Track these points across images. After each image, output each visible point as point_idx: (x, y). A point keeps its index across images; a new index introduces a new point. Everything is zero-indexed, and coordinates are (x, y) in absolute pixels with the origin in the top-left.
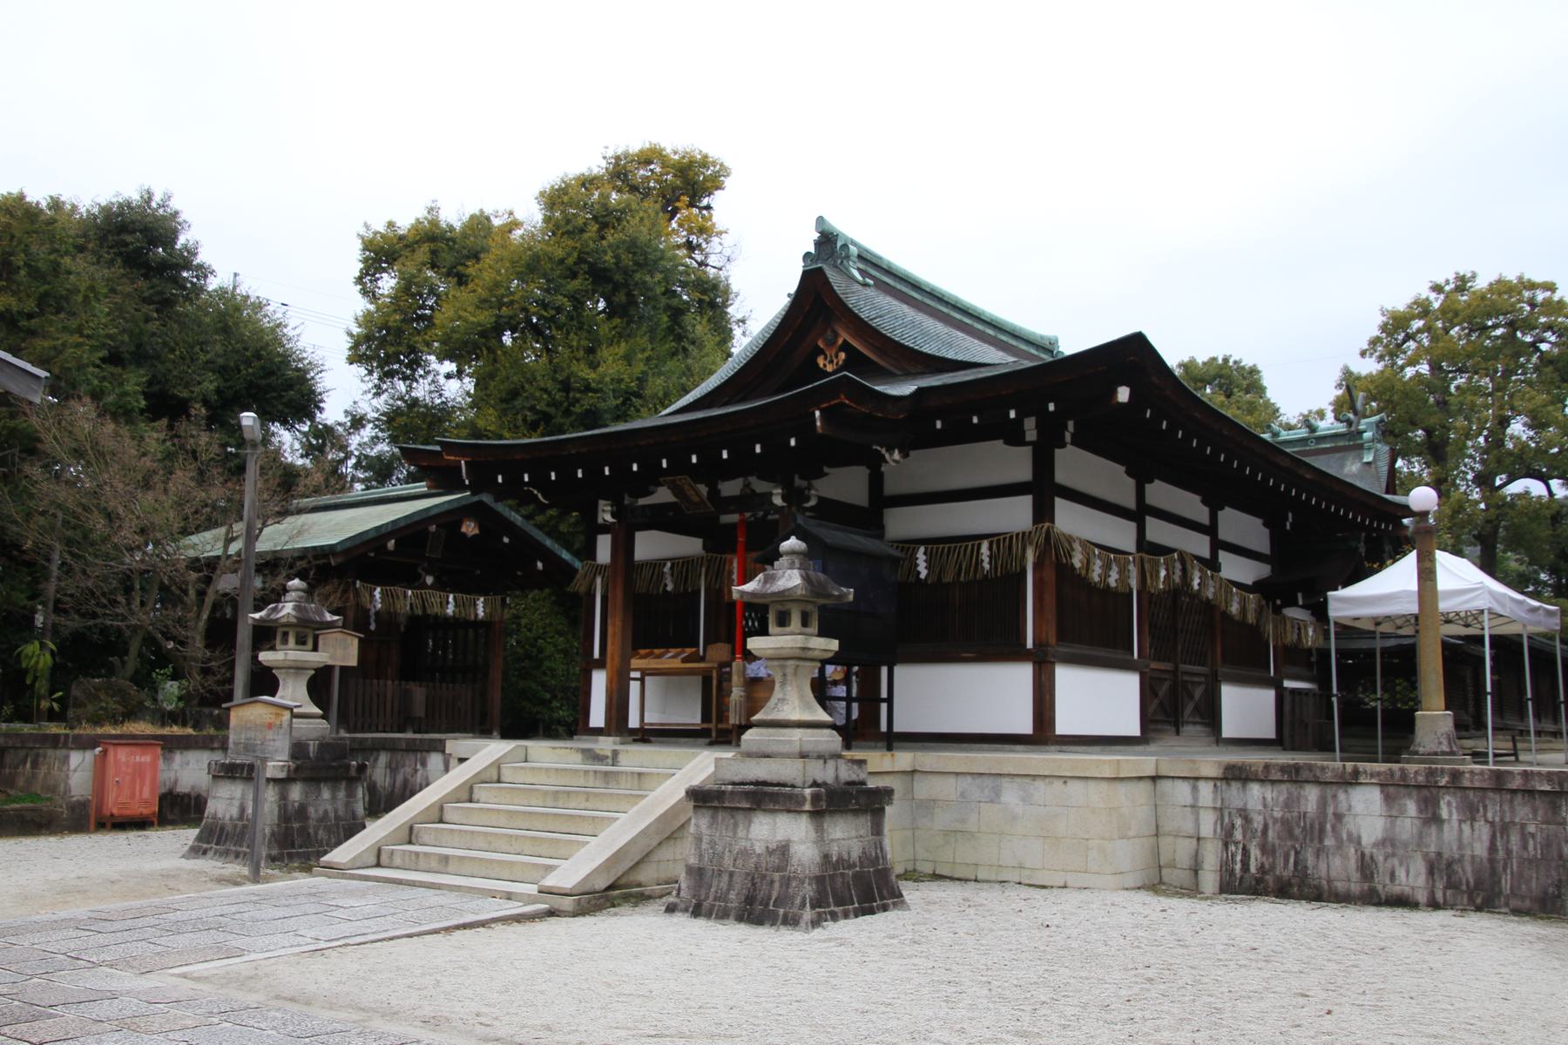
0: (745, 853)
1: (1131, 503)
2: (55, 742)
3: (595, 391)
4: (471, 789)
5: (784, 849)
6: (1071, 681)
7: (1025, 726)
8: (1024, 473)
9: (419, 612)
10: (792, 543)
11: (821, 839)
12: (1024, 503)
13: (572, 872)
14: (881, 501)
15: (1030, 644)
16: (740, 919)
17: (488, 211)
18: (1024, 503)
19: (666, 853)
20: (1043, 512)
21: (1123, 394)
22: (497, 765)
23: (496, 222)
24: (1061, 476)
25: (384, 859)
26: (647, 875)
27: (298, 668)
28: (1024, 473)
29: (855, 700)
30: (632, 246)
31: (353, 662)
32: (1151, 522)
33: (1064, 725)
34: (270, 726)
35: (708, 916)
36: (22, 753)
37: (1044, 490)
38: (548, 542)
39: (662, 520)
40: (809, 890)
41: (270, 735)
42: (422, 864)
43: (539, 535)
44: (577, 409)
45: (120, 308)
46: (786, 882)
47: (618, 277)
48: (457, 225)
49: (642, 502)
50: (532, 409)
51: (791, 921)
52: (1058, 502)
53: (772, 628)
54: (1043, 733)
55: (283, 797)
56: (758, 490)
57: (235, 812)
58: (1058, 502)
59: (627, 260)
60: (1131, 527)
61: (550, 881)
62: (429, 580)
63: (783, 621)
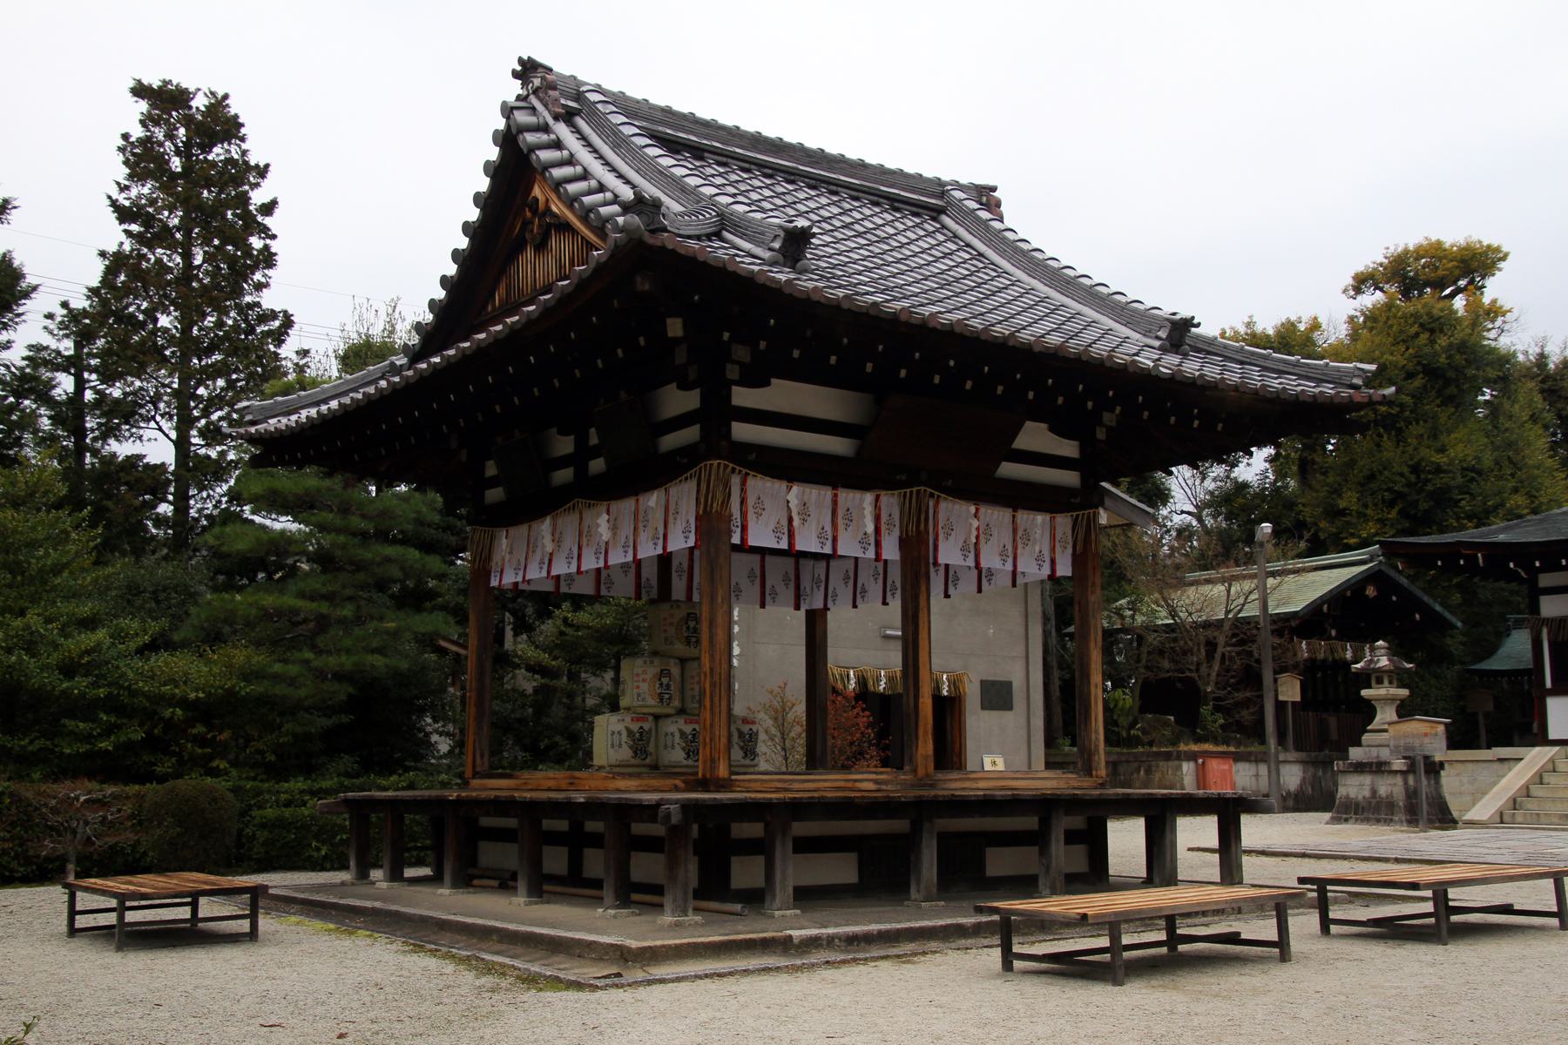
2: (1168, 756)
3: (1445, 472)
4: (1541, 777)
17: (1293, 318)
22: (1552, 760)
23: (1302, 327)
25: (1506, 818)
27: (1388, 700)
29: (121, 917)
30: (1462, 347)
31: (1298, 699)
33: (1549, 884)
34: (1426, 735)
36: (1136, 765)
38: (1426, 598)
41: (1427, 740)
42: (1543, 820)
43: (1419, 593)
44: (1429, 487)
45: (1376, 505)
47: (1451, 374)
48: (1271, 332)
50: (1389, 490)
55: (1406, 783)
56: (554, 209)
57: (1367, 793)
59: (1459, 359)
62: (1333, 633)
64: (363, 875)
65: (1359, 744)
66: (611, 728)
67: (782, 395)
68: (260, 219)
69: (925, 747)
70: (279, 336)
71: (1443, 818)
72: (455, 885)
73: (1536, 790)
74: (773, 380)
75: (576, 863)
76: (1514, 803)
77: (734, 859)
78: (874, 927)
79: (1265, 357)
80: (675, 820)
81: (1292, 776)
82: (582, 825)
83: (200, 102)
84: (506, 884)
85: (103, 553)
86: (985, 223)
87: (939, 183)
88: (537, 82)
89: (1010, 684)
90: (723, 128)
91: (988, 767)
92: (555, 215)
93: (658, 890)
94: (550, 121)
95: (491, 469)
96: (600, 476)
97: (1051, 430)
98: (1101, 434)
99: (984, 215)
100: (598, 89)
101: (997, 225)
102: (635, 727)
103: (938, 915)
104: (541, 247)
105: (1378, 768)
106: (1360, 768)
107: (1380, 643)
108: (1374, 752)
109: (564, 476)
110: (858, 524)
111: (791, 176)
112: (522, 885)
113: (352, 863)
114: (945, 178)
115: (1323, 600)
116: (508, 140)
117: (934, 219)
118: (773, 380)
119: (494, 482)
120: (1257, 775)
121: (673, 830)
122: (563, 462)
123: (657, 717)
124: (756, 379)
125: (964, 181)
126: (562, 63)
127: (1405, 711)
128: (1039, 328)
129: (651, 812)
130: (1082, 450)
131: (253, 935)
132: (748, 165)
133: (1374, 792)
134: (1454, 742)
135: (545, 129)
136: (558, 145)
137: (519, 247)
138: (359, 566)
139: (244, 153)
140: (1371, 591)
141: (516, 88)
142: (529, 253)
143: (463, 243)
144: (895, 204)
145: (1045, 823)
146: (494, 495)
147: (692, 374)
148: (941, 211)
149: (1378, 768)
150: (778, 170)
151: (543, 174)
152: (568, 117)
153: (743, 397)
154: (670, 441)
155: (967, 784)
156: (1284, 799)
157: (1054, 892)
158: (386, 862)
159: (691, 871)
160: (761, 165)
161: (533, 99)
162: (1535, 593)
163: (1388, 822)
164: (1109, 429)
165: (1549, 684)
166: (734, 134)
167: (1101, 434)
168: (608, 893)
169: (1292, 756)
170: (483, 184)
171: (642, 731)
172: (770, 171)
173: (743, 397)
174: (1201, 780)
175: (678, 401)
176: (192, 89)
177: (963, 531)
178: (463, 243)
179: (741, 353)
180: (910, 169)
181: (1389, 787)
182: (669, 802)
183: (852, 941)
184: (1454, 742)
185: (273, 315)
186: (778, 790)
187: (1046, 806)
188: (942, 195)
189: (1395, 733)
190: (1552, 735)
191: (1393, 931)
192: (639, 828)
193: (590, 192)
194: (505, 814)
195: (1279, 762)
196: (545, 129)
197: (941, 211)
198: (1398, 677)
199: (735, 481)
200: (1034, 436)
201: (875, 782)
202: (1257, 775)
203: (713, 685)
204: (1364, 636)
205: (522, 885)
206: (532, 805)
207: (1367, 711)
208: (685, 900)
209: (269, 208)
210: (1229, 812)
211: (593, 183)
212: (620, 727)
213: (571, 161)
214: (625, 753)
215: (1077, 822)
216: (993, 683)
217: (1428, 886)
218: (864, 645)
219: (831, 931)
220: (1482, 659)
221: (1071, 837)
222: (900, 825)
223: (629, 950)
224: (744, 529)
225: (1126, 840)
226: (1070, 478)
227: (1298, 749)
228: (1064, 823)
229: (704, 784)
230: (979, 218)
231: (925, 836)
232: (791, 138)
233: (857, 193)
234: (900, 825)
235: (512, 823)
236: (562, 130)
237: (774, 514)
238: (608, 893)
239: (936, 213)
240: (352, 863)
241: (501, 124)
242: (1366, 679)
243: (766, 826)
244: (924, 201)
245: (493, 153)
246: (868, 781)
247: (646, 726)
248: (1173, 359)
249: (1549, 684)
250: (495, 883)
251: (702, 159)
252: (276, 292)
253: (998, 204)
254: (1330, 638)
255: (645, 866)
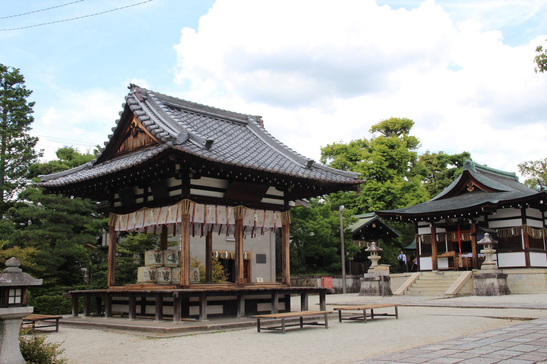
0: (485, 285)
1: (541, 217)
5: (493, 284)
6: (532, 255)
7: (524, 265)
8: (520, 214)
9: (168, 244)
10: (486, 234)
11: (498, 282)
12: (520, 220)
13: (451, 290)
14: (487, 220)
15: (523, 248)
16: (486, 295)
18: (520, 220)
19: (463, 289)
20: (524, 222)
21: (542, 202)
24: (527, 214)
26: (461, 292)
28: (520, 214)
32: (541, 226)
33: (532, 264)
35: (480, 295)
37: (524, 218)
39: (441, 226)
40: (498, 290)
46: (494, 289)
49: (437, 223)
51: (495, 295)
52: (527, 220)
53: (484, 248)
54: (528, 266)
55: (379, 284)
56: (140, 126)
57: (369, 287)
58: (527, 220)
60: (542, 222)
61: (447, 293)
63: (486, 246)
64: (76, 315)
65: (367, 273)
66: (144, 271)
67: (204, 181)
68: (29, 107)
69: (241, 275)
70: (33, 145)
71: (389, 293)
72: (108, 317)
73: (413, 285)
74: (202, 177)
75: (143, 310)
76: (408, 289)
77: (190, 307)
78: (228, 324)
79: (333, 170)
80: (177, 296)
81: (350, 282)
82: (145, 298)
83: (10, 70)
84: (124, 315)
85: (171, 260)
86: (259, 129)
87: (246, 116)
88: (135, 91)
89: (265, 255)
90: (186, 102)
91: (258, 281)
92: (140, 128)
93: (172, 316)
94: (139, 102)
95: (117, 196)
96: (151, 202)
97: (277, 189)
98: (290, 190)
99: (259, 126)
100: (152, 93)
101: (262, 129)
102: (151, 271)
103: (244, 321)
104: (135, 136)
105: (372, 279)
106: (367, 280)
107: (373, 243)
108: (371, 275)
109: (140, 200)
110: (224, 215)
111: (205, 115)
112: (130, 316)
113: (73, 312)
114: (248, 114)
115: (360, 228)
116: (127, 107)
117: (244, 126)
118: (202, 177)
119: (117, 200)
120: (339, 283)
121: (176, 299)
122: (140, 196)
123: (172, 268)
124: (197, 177)
125: (253, 115)
126: (143, 85)
127: (380, 262)
128: (272, 165)
129: (170, 294)
130: (285, 194)
131: (57, 331)
132: (193, 112)
133: (371, 287)
134: (391, 272)
135: (138, 104)
136: (141, 109)
137: (128, 135)
138: (68, 222)
139: (24, 87)
140: (374, 226)
141: (129, 91)
142: (131, 137)
143: (112, 133)
144: (234, 122)
145: (273, 297)
146: (118, 204)
147: (180, 176)
148: (247, 124)
149: (372, 279)
150: (201, 113)
151: (137, 118)
152: (144, 101)
153: (193, 182)
154: (173, 193)
155: (253, 286)
156: (347, 289)
157: (275, 313)
158: (85, 311)
159: (180, 310)
160: (196, 112)
161: (134, 95)
162: (417, 227)
163: (374, 295)
164: (292, 188)
165: (420, 254)
166: (189, 103)
167: (290, 190)
168: (157, 317)
169: (351, 276)
170: (119, 118)
171: (153, 272)
172: (199, 114)
173: (193, 182)
174: (323, 284)
175: (175, 182)
176: (7, 66)
177: (252, 217)
178: (112, 133)
179: (194, 171)
180: (238, 112)
181: (375, 285)
182: (176, 292)
183: (223, 327)
184: (391, 272)
185: (33, 138)
186: (202, 288)
187: (273, 292)
188: (247, 119)
189: (378, 270)
190: (421, 269)
191: (356, 319)
192: (166, 299)
193: (151, 125)
194: (124, 296)
195: (346, 278)
196: (138, 104)
197: (247, 124)
198: (379, 253)
199: (192, 204)
200: (272, 191)
201: (228, 286)
202: (339, 283)
203: (185, 260)
204: (369, 239)
205: (130, 316)
206: (134, 293)
207: (370, 262)
208: (179, 317)
209: (32, 104)
210: (323, 293)
211: (157, 126)
212: (147, 271)
213: (145, 114)
214: (148, 279)
215: (282, 296)
216: (260, 255)
217: (362, 309)
218: (223, 246)
219: (217, 325)
220: (407, 245)
221: (280, 300)
222: (234, 297)
223: (166, 330)
224: (193, 218)
225: (295, 301)
226: (281, 202)
227: (352, 274)
228: (278, 296)
229: (182, 287)
230: (257, 127)
231: (241, 300)
232: (205, 104)
233: (223, 119)
234: (234, 297)
235: (127, 299)
236: (142, 105)
237: (201, 214)
238: (157, 317)
239: (245, 124)
240: (73, 312)
241: (125, 102)
242: (369, 253)
243: (200, 298)
244: (241, 122)
245: (122, 110)
246: (224, 285)
247: (168, 271)
248: (308, 172)
249: (420, 254)
250: (120, 316)
251: (180, 111)
252: (33, 131)
253: (262, 122)
254: (362, 240)
255: (167, 310)
